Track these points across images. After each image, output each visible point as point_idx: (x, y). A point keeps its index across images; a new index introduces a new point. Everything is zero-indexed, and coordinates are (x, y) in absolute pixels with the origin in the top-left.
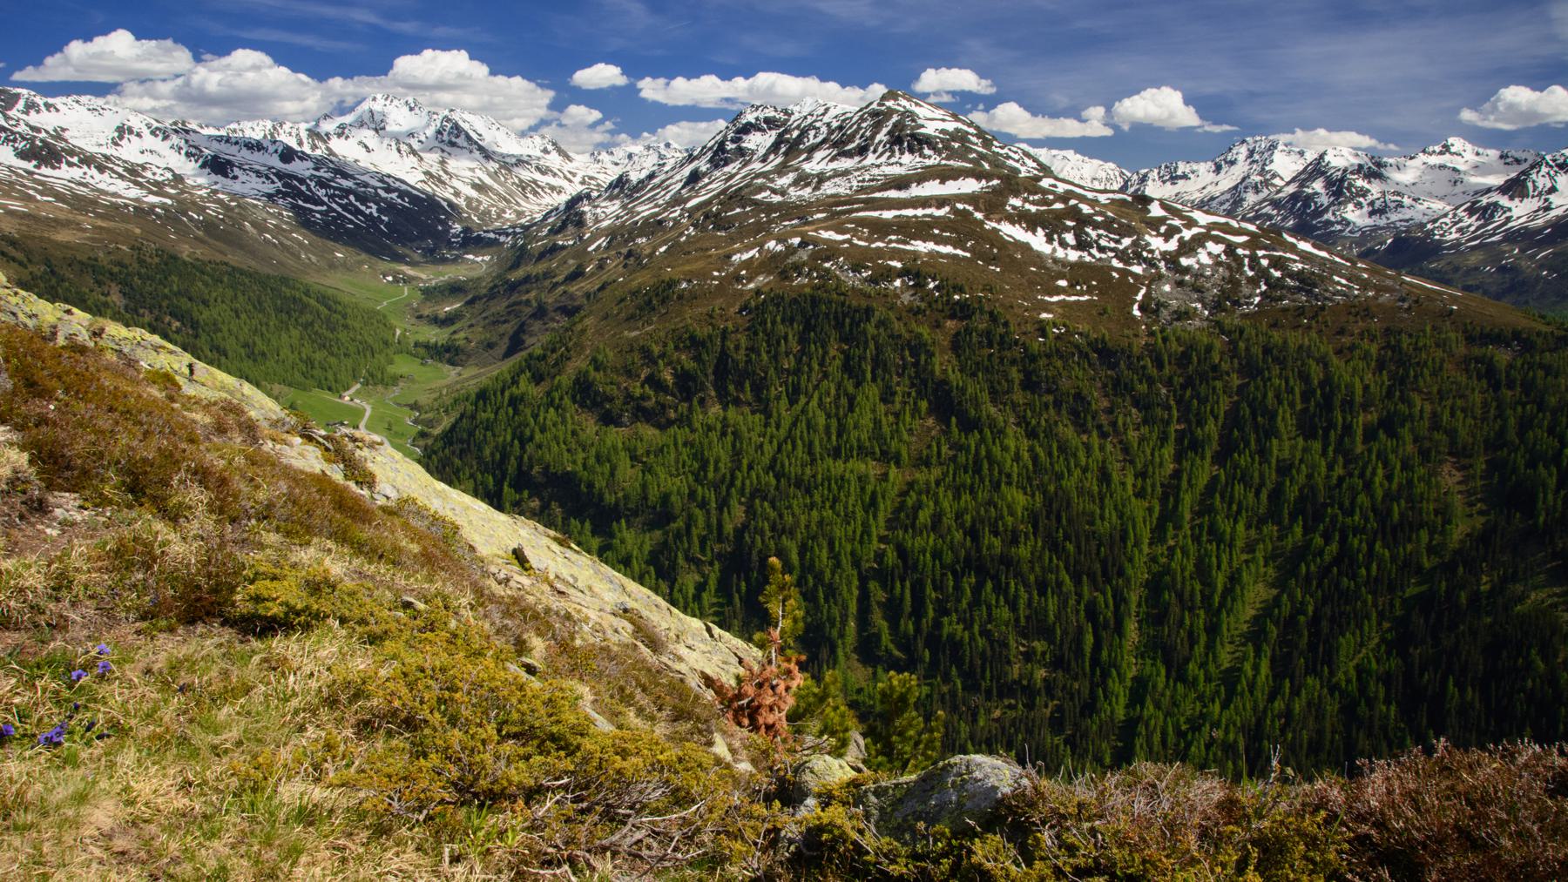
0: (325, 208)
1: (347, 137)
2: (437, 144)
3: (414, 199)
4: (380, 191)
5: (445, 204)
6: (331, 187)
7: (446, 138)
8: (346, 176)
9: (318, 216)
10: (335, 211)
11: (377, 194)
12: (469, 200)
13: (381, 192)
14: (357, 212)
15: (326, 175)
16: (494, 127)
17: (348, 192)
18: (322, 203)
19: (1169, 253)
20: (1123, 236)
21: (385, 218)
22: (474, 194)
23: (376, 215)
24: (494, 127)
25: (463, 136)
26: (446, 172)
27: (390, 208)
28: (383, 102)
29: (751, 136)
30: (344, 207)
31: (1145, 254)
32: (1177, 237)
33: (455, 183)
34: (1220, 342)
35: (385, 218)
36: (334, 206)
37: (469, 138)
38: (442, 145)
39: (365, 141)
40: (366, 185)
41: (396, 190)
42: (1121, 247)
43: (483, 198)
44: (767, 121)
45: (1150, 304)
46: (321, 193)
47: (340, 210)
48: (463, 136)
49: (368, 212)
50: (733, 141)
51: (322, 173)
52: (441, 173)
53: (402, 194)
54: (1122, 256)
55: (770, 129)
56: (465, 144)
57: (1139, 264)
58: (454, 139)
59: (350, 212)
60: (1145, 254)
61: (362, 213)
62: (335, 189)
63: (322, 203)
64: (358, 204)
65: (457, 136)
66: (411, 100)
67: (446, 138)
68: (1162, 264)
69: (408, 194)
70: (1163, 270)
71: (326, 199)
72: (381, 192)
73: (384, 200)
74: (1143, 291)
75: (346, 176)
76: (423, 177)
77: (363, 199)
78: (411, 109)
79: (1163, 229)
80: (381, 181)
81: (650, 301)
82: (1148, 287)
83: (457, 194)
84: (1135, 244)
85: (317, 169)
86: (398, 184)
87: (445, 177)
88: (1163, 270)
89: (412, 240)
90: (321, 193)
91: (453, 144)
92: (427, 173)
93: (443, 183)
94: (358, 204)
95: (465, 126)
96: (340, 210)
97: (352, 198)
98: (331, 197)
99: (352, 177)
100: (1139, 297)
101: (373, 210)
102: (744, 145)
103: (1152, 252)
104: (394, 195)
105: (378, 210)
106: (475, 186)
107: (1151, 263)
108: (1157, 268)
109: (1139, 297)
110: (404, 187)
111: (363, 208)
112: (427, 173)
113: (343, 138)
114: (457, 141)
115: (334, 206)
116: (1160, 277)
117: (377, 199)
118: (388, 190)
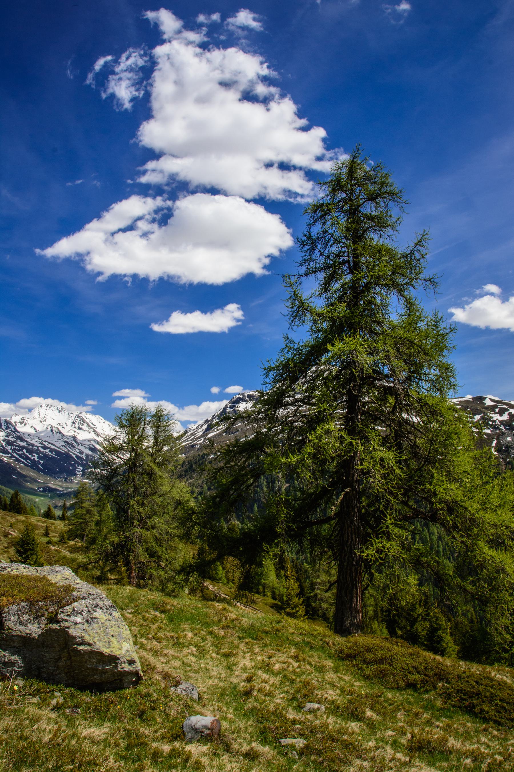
0: (10, 455)
1: (25, 424)
2: (72, 428)
3: (58, 453)
4: (40, 449)
5: (74, 456)
6: (14, 445)
7: (77, 425)
8: (22, 440)
9: (5, 459)
10: (15, 457)
11: (38, 449)
12: (87, 456)
13: (41, 449)
14: (27, 458)
15: (12, 439)
16: (102, 422)
17: (23, 447)
18: (9, 453)
19: (505, 421)
20: (474, 414)
21: (42, 462)
22: (90, 453)
23: (37, 460)
24: (102, 422)
25: (86, 425)
26: (76, 442)
27: (45, 457)
28: (45, 408)
29: (240, 405)
30: (20, 456)
31: (490, 423)
32: (507, 413)
33: (81, 447)
34: (452, 734)
35: (42, 462)
36: (15, 455)
37: (88, 425)
38: (74, 429)
39: (35, 426)
40: (33, 445)
41: (47, 448)
42: (475, 420)
43: (94, 455)
44: (249, 396)
45: (501, 448)
46: (8, 448)
47: (18, 457)
48: (86, 425)
49: (32, 458)
50: (230, 407)
51: (10, 438)
52: (73, 442)
53: (52, 450)
54: (477, 425)
55: (251, 400)
56: (87, 429)
57: (489, 429)
58: (81, 426)
59: (23, 458)
60: (490, 423)
61: (30, 459)
62: (16, 446)
63: (9, 453)
64: (28, 454)
65: (83, 425)
66: (60, 407)
67: (77, 425)
68: (502, 427)
69: (54, 450)
70: (504, 430)
71: (10, 451)
72: (41, 449)
73: (42, 453)
74: (495, 442)
75: (22, 440)
76: (63, 444)
77: (31, 452)
78: (60, 412)
79: (497, 410)
80: (41, 443)
81: (191, 466)
82: (497, 439)
83: (81, 452)
84: (482, 418)
85: (7, 436)
86: (50, 445)
87: (75, 444)
88: (504, 430)
89: (55, 474)
90: (8, 448)
91: (80, 429)
92: (65, 442)
93: (74, 447)
94: (28, 454)
95: (88, 421)
96: (18, 457)
97: (25, 451)
98: (14, 450)
99: (26, 441)
100: (494, 444)
101: (36, 457)
102: (236, 409)
103: (495, 421)
104: (47, 451)
105: (38, 458)
106: (91, 449)
107: (495, 427)
108: (500, 429)
109: (494, 444)
110: (53, 447)
111: (30, 456)
112: (65, 442)
113: (23, 425)
114: (83, 427)
115: (15, 455)
116: (503, 434)
117: (38, 452)
118: (45, 447)
